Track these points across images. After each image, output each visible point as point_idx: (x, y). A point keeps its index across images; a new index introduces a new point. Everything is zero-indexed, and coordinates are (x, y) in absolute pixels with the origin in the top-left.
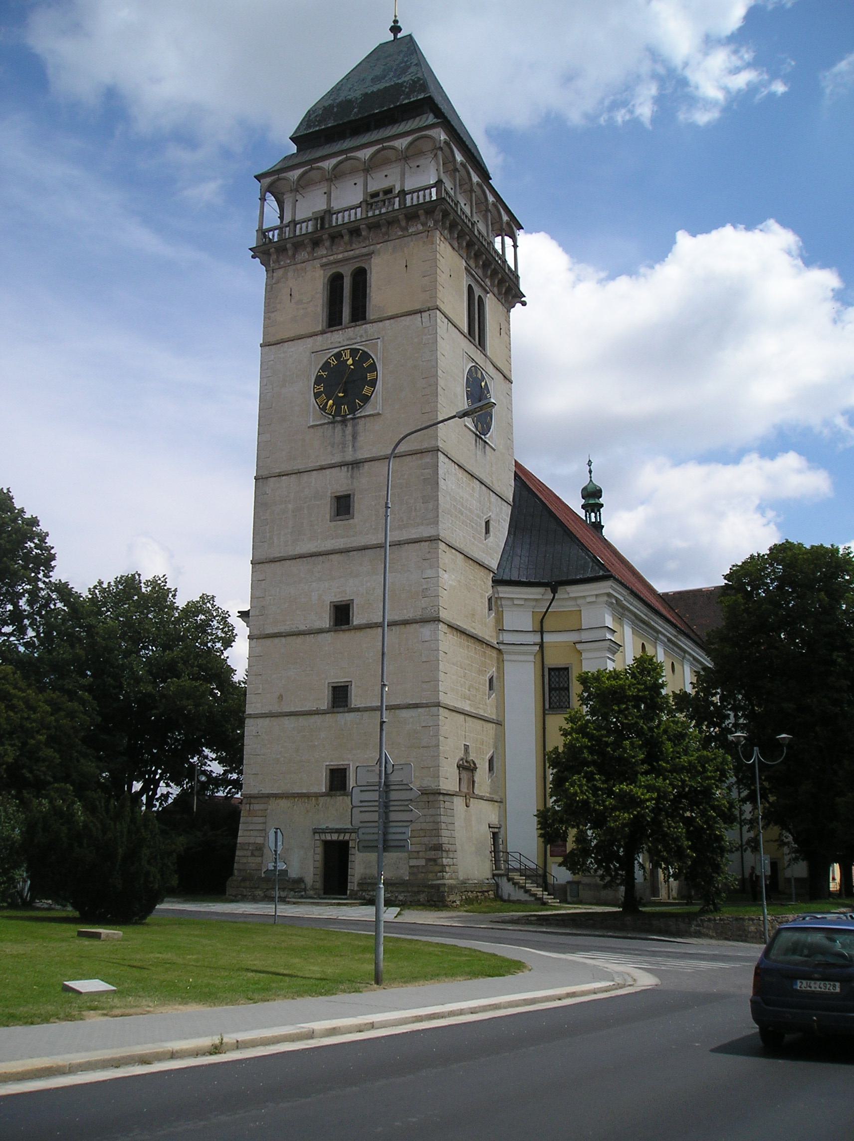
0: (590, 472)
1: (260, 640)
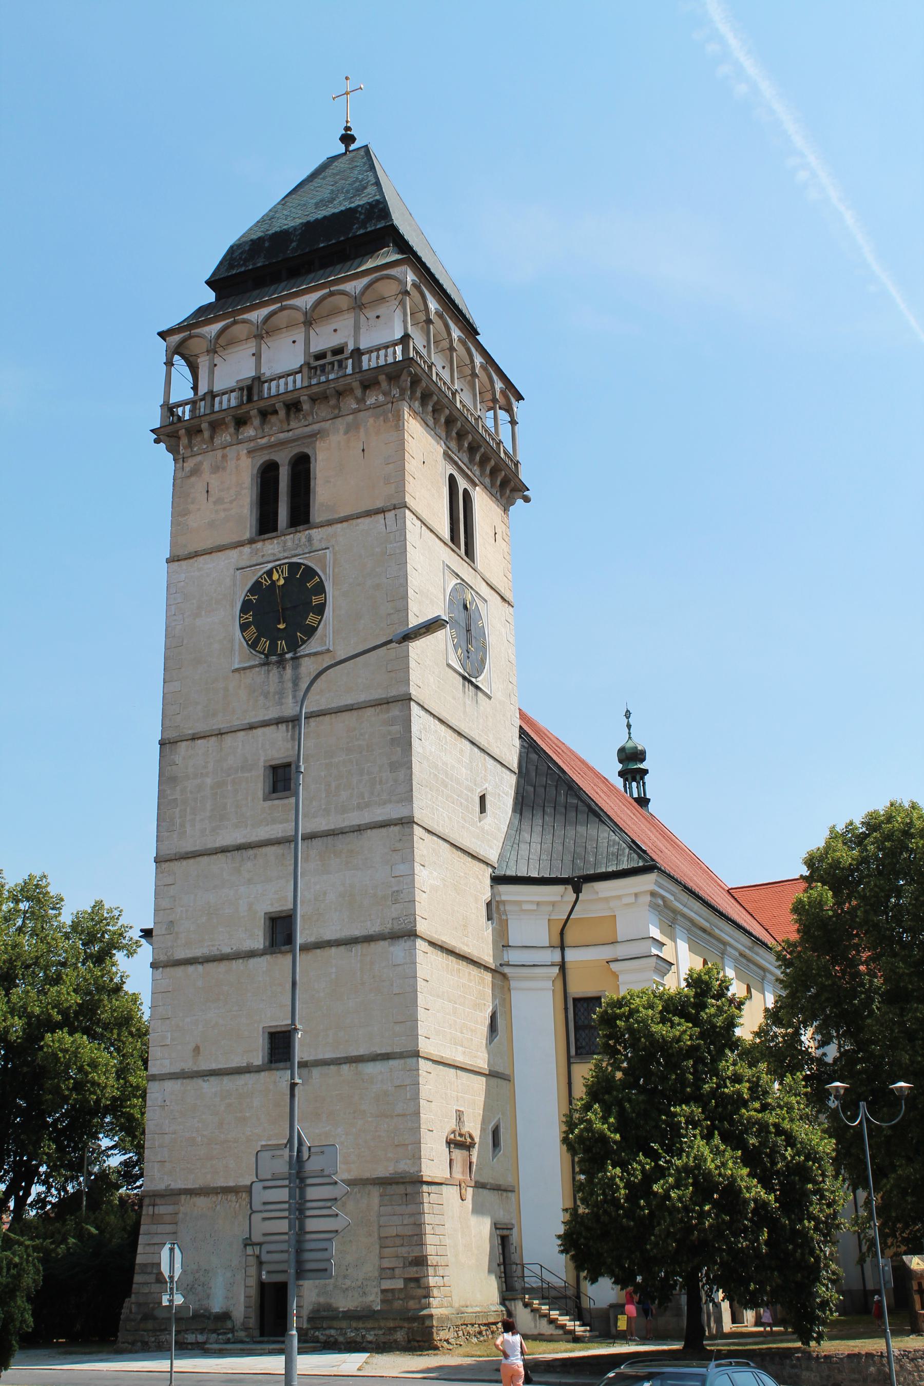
0: (629, 726)
1: (168, 969)
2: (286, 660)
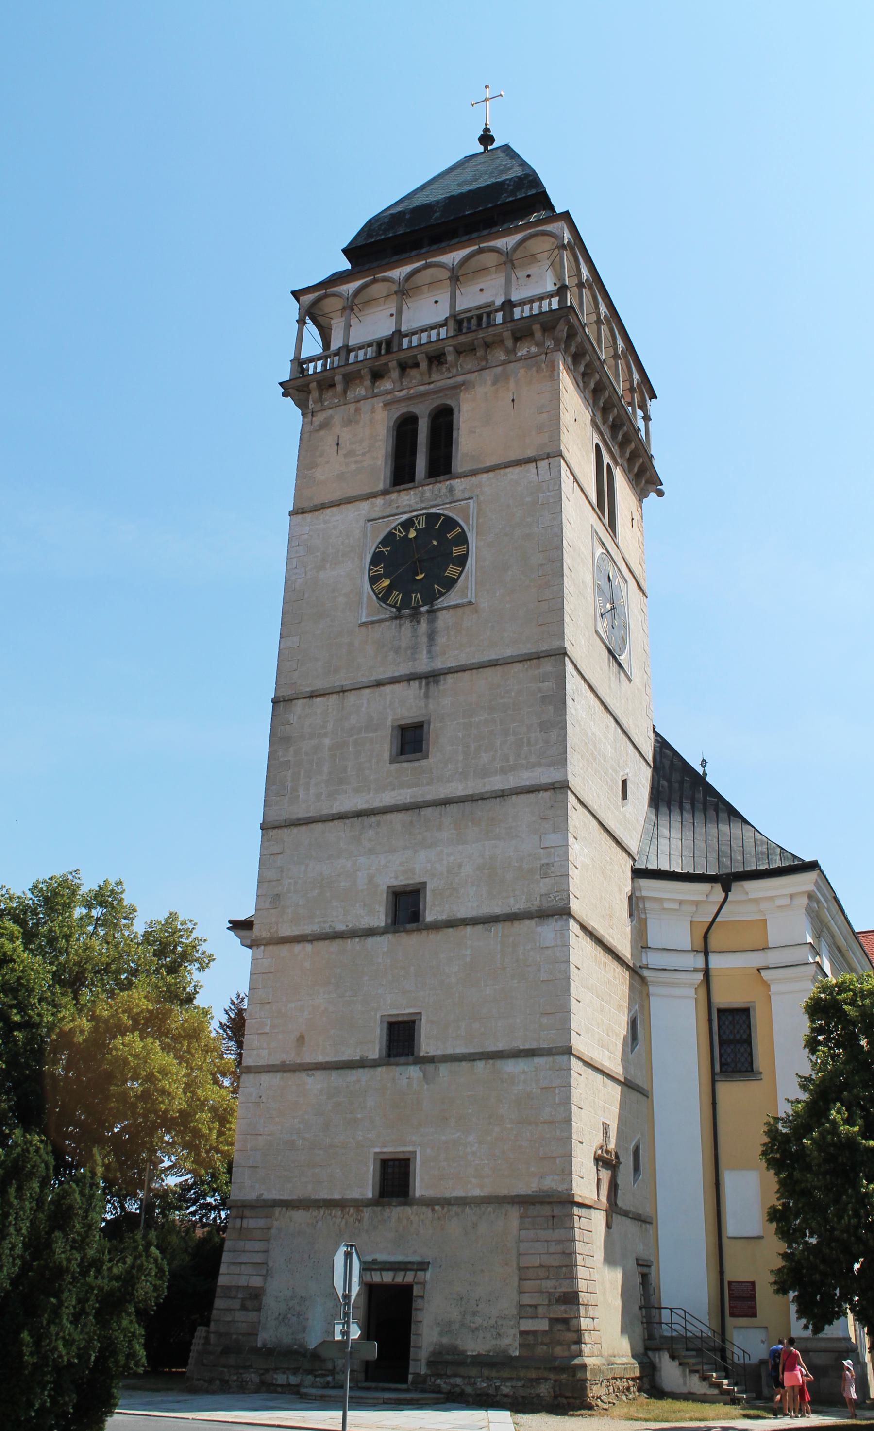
1: (271, 947)
2: (421, 613)
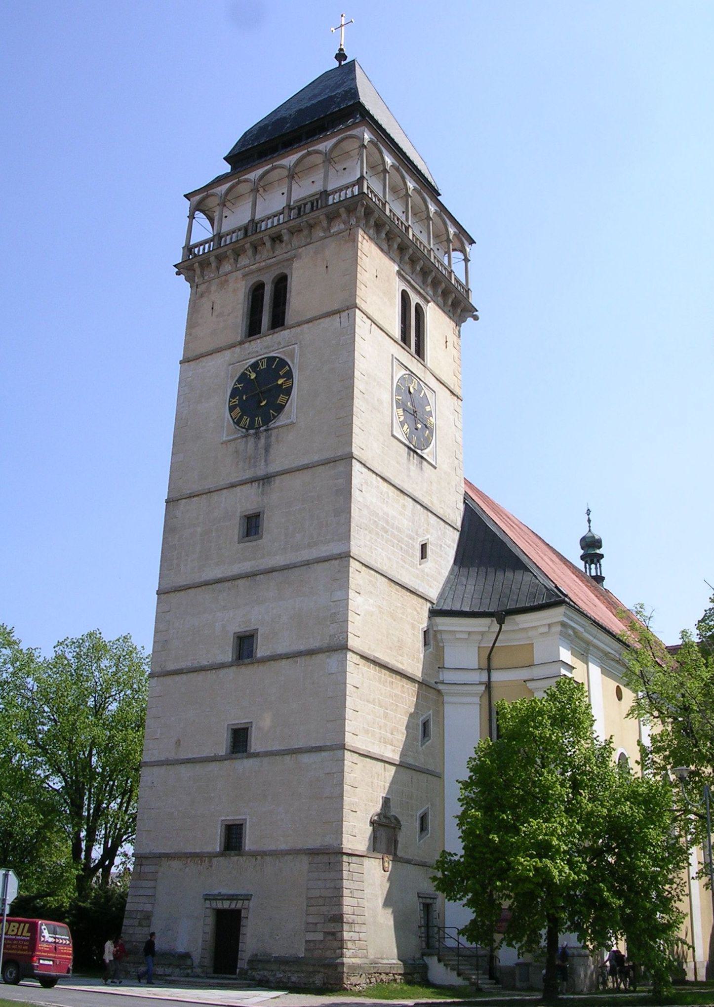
0: (589, 521)
1: (161, 678)
